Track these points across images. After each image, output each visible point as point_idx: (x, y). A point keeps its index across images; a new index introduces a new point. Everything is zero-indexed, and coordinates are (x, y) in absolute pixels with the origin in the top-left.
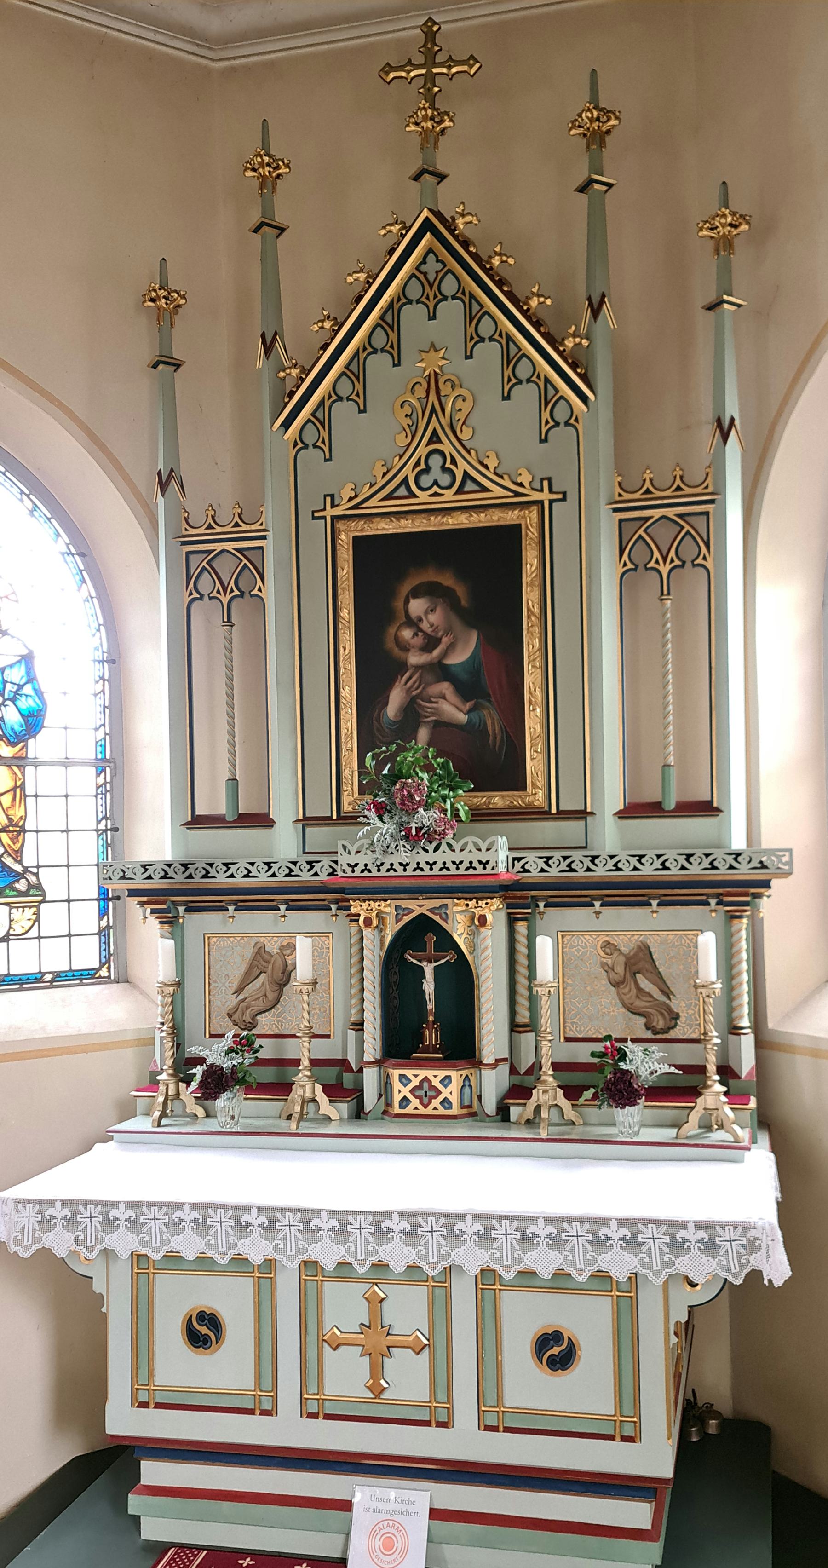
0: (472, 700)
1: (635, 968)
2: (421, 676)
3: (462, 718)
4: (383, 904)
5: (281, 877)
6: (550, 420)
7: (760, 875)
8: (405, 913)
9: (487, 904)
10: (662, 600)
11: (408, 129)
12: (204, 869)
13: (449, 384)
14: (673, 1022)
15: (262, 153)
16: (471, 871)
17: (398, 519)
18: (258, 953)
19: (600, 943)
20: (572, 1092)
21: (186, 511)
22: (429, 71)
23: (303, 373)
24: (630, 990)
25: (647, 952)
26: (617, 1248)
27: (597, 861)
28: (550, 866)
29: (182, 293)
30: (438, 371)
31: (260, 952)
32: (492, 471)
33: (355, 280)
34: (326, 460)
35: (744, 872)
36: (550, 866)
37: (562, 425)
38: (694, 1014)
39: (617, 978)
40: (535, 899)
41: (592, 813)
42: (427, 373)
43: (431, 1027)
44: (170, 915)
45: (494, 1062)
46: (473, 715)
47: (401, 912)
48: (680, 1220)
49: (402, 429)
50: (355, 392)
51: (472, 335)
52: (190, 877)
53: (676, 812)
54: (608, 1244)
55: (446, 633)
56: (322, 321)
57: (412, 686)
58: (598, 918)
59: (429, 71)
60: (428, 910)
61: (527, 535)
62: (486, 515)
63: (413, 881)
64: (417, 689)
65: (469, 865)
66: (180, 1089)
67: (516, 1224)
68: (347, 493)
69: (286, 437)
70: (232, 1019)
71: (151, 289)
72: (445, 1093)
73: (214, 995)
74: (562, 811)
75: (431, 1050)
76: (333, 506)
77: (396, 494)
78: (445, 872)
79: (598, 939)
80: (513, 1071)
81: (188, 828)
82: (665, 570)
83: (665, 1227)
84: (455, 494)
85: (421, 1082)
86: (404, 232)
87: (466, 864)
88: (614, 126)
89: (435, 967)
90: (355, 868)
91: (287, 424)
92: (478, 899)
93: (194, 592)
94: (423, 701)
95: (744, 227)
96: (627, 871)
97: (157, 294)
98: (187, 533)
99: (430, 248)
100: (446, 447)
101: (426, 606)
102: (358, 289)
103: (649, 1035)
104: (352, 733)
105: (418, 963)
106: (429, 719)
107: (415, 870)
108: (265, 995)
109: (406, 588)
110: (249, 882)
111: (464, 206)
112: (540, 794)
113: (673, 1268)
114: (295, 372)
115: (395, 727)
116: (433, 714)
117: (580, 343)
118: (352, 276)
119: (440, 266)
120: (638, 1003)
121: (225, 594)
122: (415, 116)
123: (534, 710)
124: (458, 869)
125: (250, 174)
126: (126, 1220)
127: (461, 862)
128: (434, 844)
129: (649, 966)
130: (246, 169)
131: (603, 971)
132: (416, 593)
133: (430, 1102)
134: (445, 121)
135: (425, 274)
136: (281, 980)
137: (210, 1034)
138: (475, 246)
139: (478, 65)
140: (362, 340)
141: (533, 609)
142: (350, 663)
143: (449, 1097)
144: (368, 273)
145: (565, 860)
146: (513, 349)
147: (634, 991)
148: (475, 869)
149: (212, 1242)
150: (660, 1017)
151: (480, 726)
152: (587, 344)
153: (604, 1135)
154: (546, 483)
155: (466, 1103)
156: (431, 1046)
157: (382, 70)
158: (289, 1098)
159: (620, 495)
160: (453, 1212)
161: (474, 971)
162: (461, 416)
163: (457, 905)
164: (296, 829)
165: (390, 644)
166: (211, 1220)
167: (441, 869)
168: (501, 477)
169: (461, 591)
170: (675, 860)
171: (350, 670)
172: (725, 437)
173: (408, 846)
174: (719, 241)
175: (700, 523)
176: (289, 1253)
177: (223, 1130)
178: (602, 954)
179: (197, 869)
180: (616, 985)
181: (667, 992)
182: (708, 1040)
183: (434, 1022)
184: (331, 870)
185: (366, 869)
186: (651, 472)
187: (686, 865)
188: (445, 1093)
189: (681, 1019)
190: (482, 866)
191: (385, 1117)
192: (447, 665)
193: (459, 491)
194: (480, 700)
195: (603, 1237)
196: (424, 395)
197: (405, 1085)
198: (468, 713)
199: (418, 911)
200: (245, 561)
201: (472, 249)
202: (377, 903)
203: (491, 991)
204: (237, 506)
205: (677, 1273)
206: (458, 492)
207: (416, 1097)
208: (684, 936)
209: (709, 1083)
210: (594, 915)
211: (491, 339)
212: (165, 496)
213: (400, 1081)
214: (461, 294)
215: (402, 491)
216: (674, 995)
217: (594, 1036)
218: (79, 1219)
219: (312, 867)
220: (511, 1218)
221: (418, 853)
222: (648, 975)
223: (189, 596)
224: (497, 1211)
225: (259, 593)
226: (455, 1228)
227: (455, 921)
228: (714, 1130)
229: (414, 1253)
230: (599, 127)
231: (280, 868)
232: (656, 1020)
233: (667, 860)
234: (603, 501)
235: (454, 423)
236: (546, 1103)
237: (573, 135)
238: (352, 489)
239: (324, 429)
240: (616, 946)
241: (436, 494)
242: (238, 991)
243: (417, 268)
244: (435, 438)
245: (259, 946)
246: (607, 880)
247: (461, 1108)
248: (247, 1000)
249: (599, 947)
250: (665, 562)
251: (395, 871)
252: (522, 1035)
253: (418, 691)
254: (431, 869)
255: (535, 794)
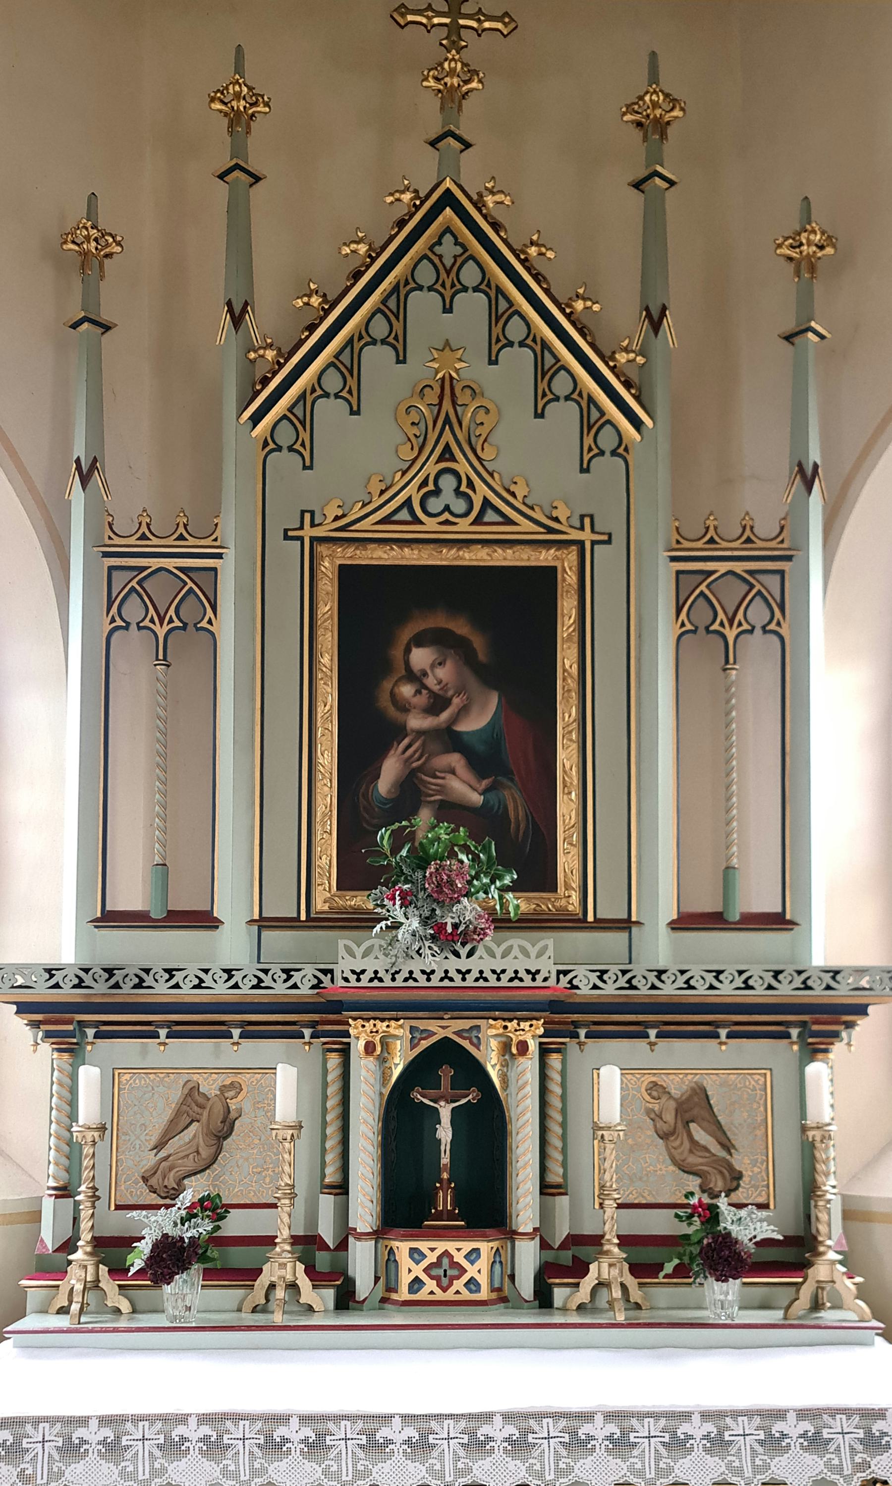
0: (491, 777)
1: (687, 1116)
2: (424, 745)
3: (477, 799)
4: (393, 1023)
5: (245, 990)
6: (593, 447)
7: (858, 999)
8: (424, 1036)
9: (531, 1026)
10: (725, 670)
11: (425, 84)
12: (137, 976)
13: (468, 392)
14: (735, 1184)
15: (241, 81)
16: (516, 983)
17: (401, 548)
18: (190, 1094)
19: (646, 1083)
20: (639, 1270)
21: (109, 515)
22: (454, 22)
23: (282, 357)
24: (682, 1143)
25: (703, 1096)
26: (795, 1449)
27: (664, 977)
28: (605, 982)
29: (119, 238)
30: (454, 375)
31: (192, 1093)
32: (521, 501)
33: (352, 251)
34: (305, 468)
35: (842, 993)
36: (605, 982)
37: (608, 454)
38: (761, 1172)
39: (665, 1128)
40: (576, 1024)
41: (638, 923)
42: (440, 375)
43: (445, 1185)
44: (75, 1040)
45: (532, 1231)
46: (492, 796)
47: (417, 1035)
48: (876, 1407)
49: (407, 439)
50: (347, 388)
51: (498, 336)
52: (117, 986)
53: (742, 924)
54: (784, 1444)
55: (458, 693)
56: (309, 296)
57: (412, 756)
58: (652, 1051)
59: (454, 22)
60: (454, 1033)
61: (564, 580)
62: (514, 553)
63: (442, 993)
64: (419, 759)
65: (514, 975)
66: (100, 1273)
67: (663, 1422)
68: (332, 511)
69: (254, 434)
70: (149, 1184)
71: (81, 225)
72: (471, 1271)
73: (124, 1152)
74: (599, 919)
75: (445, 1217)
76: (313, 525)
77: (396, 518)
78: (481, 983)
79: (643, 1079)
80: (544, 1245)
81: (96, 927)
82: (731, 634)
83: (858, 1418)
84: (472, 524)
85: (440, 1258)
86: (418, 202)
87: (510, 974)
88: (676, 117)
89: (453, 1109)
90: (361, 976)
91: (256, 419)
92: (520, 1020)
93: (117, 618)
94: (426, 775)
95: (829, 250)
96: (701, 990)
97: (88, 233)
98: (111, 542)
99: (448, 227)
100: (462, 467)
101: (434, 657)
102: (355, 264)
103: (154, 1199)
104: (331, 811)
105: (432, 1104)
106: (432, 799)
107: (442, 980)
108: (198, 1152)
109: (407, 634)
110: (201, 996)
111: (495, 182)
112: (574, 897)
113: (868, 1472)
114: (270, 354)
115: (388, 806)
116: (439, 792)
117: (634, 360)
118: (348, 246)
119: (459, 250)
120: (692, 1159)
121: (161, 626)
122: (439, 68)
123: (570, 793)
124: (499, 979)
125: (217, 106)
126: (99, 1443)
127: (503, 971)
128: (468, 947)
129: (707, 1115)
130: (213, 100)
131: (648, 1120)
132: (419, 641)
133: (451, 1284)
134: (473, 81)
135: (440, 257)
136: (220, 1132)
137: (116, 1205)
138: (506, 231)
139: (513, 26)
140: (357, 326)
141: (569, 670)
142: (331, 722)
143: (477, 1277)
144: (370, 245)
145: (623, 975)
146: (549, 360)
147: (687, 1144)
148: (521, 980)
149: (232, 1468)
150: (719, 1177)
151: (499, 808)
152: (642, 362)
153: (696, 1318)
154: (587, 521)
155: (497, 1285)
156: (445, 1212)
157: (395, 10)
158: (257, 1283)
159: (678, 542)
160: (577, 1410)
161: (507, 1114)
162: (483, 431)
163: (491, 1027)
164: (249, 933)
165: (384, 701)
166: (230, 1436)
167: (477, 980)
168: (532, 508)
169: (478, 643)
170: (761, 978)
171: (332, 732)
172: (809, 488)
173: (436, 949)
174: (800, 263)
175: (773, 582)
176: (344, 1478)
177: (174, 1325)
178: (648, 1098)
179: (127, 976)
180: (664, 1136)
181: (727, 1146)
182: (819, 1196)
183: (449, 1181)
184: (315, 982)
185: (376, 977)
186: (715, 519)
187: (774, 983)
188: (471, 1271)
189: (744, 1179)
190: (530, 976)
191: (387, 1306)
192: (456, 731)
193: (477, 521)
194: (499, 778)
195: (777, 1435)
196: (436, 401)
197: (417, 1263)
198: (483, 793)
199: (441, 1034)
200: (190, 584)
201: (502, 234)
202: (386, 1023)
203: (529, 1140)
204: (182, 515)
205: (836, 1483)
206: (475, 522)
207: (432, 1278)
208: (749, 1077)
209: (822, 1249)
210: (648, 1046)
211: (522, 344)
212: (86, 491)
213: (411, 1256)
214: (485, 285)
215: (404, 515)
216: (736, 1150)
217: (636, 1202)
218: (25, 1445)
219: (289, 977)
220: (656, 1416)
221: (446, 958)
222: (705, 1124)
223: (111, 623)
224: (635, 1407)
225: (209, 626)
226: (580, 1432)
227: (489, 1049)
228: (826, 1309)
229: (524, 1468)
230: (661, 115)
231: (245, 977)
232: (713, 1179)
233: (750, 977)
234: (661, 545)
235: (473, 439)
236: (616, 1279)
237: (627, 122)
238: (339, 506)
239: (305, 430)
240: (665, 1088)
241: (447, 522)
242: (159, 1146)
243: (431, 249)
244: (447, 454)
245: (190, 1086)
246: (675, 1000)
247: (492, 1292)
248: (171, 1158)
249: (643, 1090)
250: (731, 625)
251: (415, 980)
252: (557, 1197)
253: (420, 762)
254: (464, 979)
255: (569, 896)
